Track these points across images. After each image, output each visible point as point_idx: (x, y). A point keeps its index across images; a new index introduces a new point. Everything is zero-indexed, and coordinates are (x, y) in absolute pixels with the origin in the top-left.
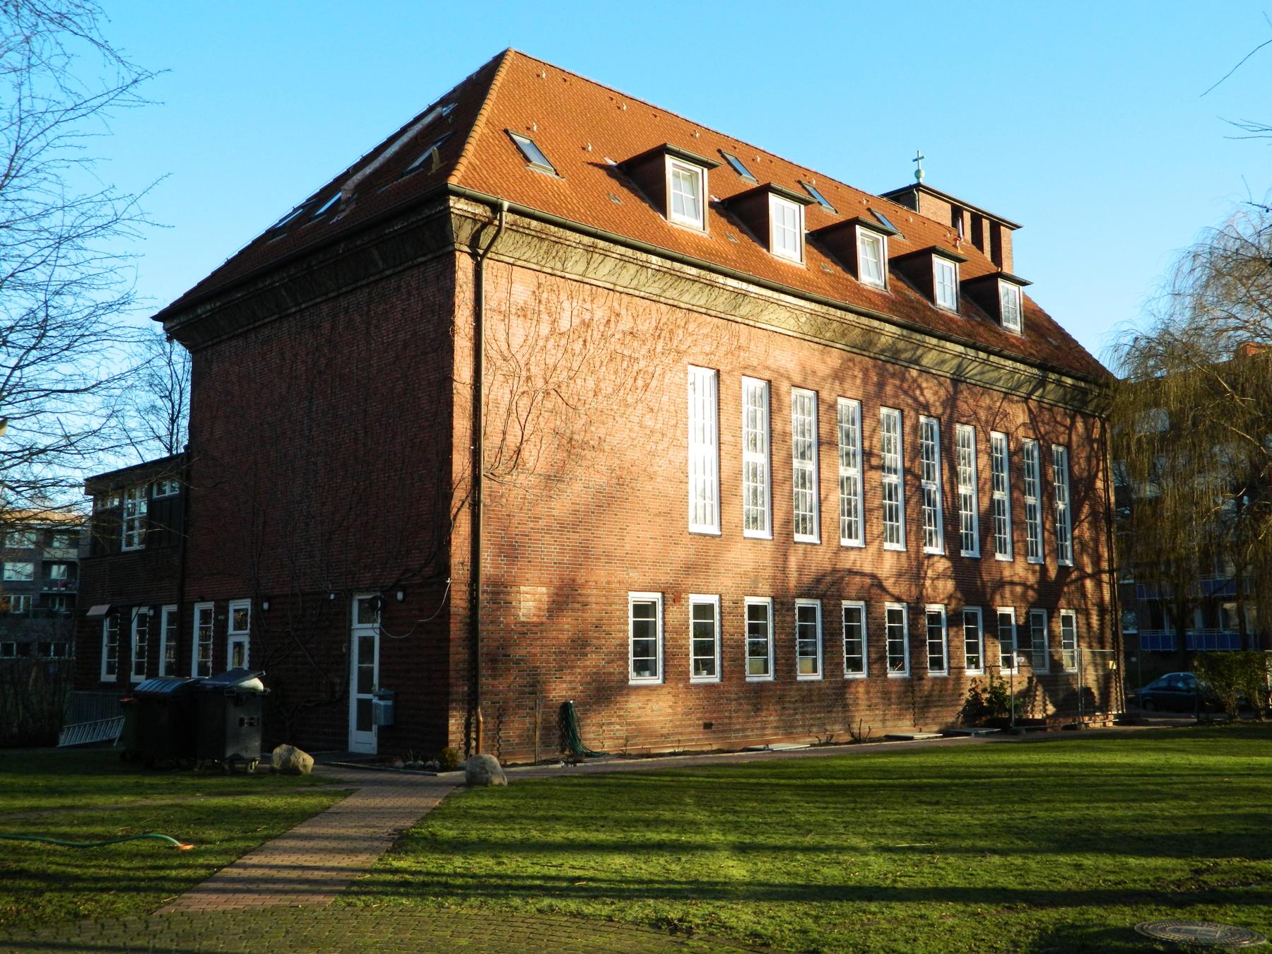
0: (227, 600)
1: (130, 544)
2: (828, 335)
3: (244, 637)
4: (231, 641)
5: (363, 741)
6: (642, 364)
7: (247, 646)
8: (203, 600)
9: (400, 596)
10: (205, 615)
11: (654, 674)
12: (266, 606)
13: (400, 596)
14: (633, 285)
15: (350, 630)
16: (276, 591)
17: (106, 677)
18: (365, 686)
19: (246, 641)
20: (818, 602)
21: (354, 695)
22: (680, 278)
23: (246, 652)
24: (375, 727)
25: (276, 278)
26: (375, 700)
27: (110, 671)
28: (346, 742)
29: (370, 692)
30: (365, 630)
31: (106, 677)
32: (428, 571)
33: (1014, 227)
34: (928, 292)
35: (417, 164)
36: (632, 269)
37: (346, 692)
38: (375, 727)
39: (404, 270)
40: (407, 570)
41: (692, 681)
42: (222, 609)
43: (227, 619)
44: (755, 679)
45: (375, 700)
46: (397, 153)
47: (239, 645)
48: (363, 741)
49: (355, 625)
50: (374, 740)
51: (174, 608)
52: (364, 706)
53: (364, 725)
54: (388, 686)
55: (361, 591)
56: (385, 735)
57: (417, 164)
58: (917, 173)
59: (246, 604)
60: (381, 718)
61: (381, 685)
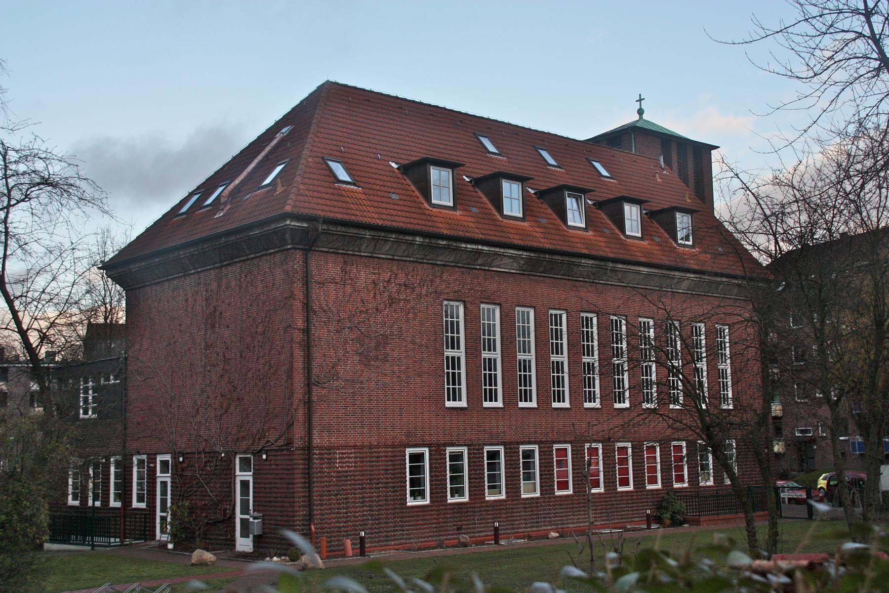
0: (156, 454)
1: (86, 413)
2: (541, 269)
3: (167, 478)
4: (158, 481)
5: (244, 544)
6: (412, 303)
7: (169, 484)
8: (139, 453)
9: (264, 457)
10: (141, 463)
11: (424, 498)
12: (181, 459)
13: (264, 457)
14: (406, 253)
15: (235, 476)
16: (188, 450)
17: (71, 502)
18: (245, 510)
19: (169, 480)
20: (537, 446)
21: (239, 516)
22: (438, 247)
23: (169, 488)
24: (251, 536)
25: (181, 253)
26: (251, 520)
27: (75, 499)
28: (234, 545)
29: (248, 514)
30: (242, 476)
31: (71, 502)
32: (281, 442)
33: (716, 147)
34: (621, 226)
35: (268, 181)
36: (404, 247)
37: (234, 513)
38: (251, 536)
39: (262, 256)
40: (268, 441)
41: (449, 501)
42: (152, 460)
43: (155, 467)
44: (492, 498)
45: (251, 520)
46: (254, 168)
47: (164, 484)
48: (244, 544)
49: (238, 473)
50: (251, 544)
51: (119, 457)
52: (245, 523)
53: (244, 535)
54: (259, 511)
55: (241, 453)
56: (258, 540)
57: (268, 181)
58: (641, 112)
59: (168, 457)
60: (257, 530)
61: (254, 511)
